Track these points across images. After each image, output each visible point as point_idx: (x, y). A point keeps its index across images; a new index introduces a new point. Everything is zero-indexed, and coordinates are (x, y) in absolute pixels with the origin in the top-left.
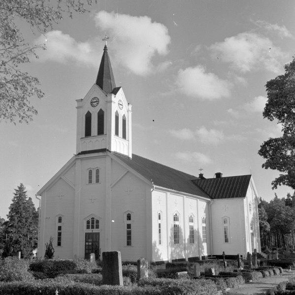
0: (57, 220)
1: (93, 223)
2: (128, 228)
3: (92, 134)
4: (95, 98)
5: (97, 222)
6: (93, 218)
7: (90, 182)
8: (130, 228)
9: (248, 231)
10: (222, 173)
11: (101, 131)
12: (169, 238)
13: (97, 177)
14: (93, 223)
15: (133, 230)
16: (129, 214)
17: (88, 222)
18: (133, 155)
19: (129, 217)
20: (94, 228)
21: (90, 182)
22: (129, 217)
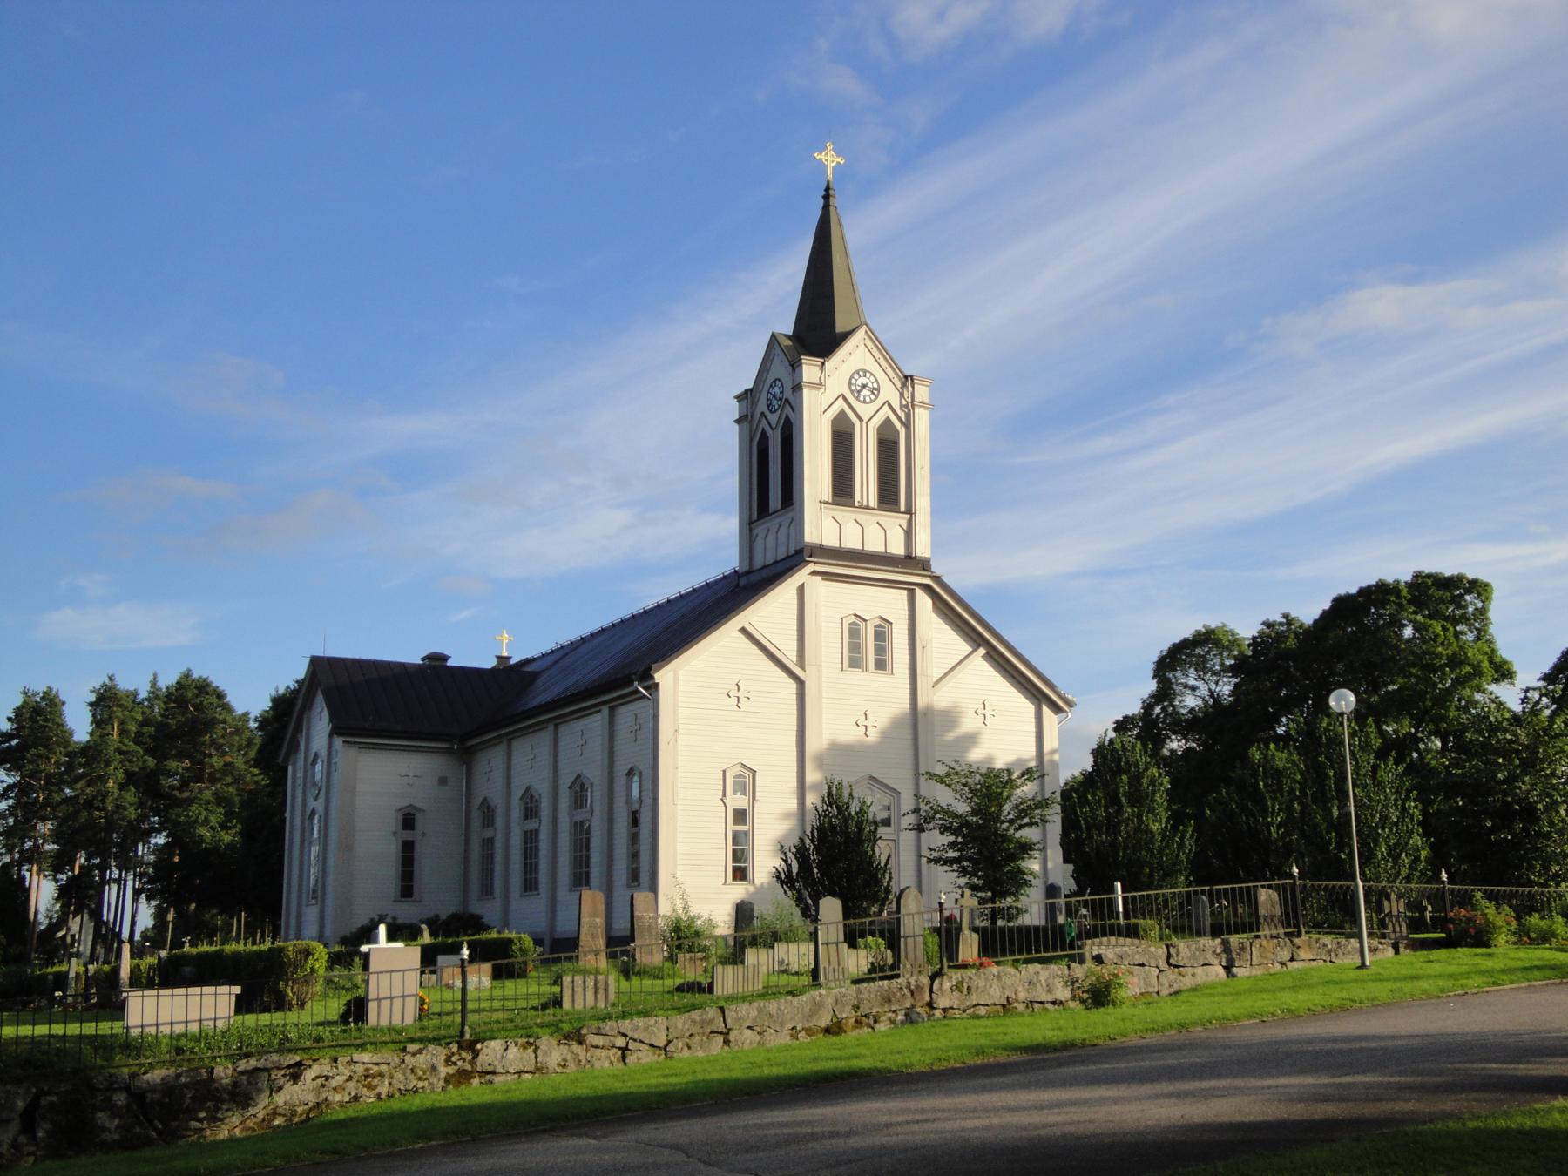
4: (865, 372)
21: (854, 663)
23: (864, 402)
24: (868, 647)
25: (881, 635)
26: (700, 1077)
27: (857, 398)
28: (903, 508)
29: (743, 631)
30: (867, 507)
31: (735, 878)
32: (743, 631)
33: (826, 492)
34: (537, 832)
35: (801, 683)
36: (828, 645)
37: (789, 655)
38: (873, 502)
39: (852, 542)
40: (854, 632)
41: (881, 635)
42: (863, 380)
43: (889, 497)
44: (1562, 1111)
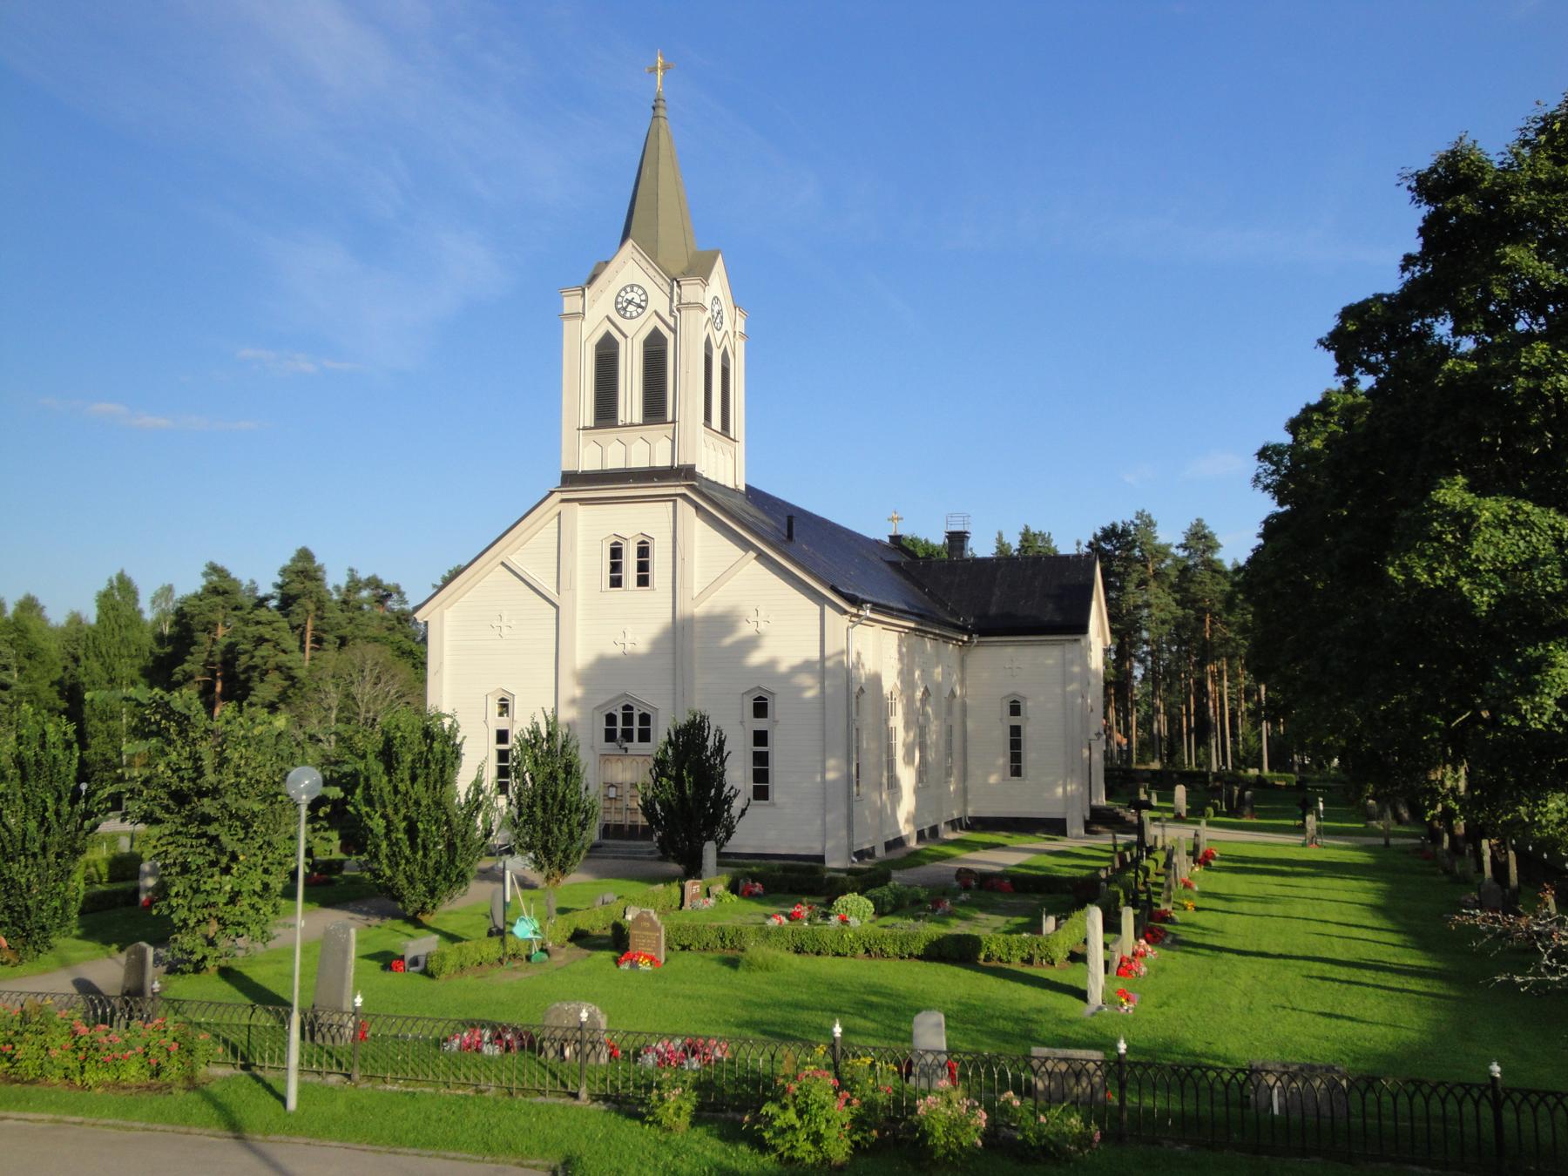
0: (1007, 710)
1: (628, 719)
2: (756, 744)
3: (622, 416)
4: (632, 286)
5: (645, 719)
6: (627, 707)
7: (616, 582)
8: (755, 753)
9: (697, 554)
10: (1122, 515)
11: (655, 408)
12: (458, 1155)
13: (643, 567)
14: (628, 719)
15: (777, 750)
16: (760, 698)
17: (611, 719)
18: (747, 487)
19: (1015, 709)
20: (630, 740)
21: (616, 582)
22: (1015, 709)
23: (631, 318)
24: (629, 565)
25: (643, 551)
26: (629, 648)
27: (624, 316)
28: (670, 418)
29: (503, 564)
30: (632, 425)
31: (766, 798)
32: (503, 564)
33: (588, 416)
34: (1064, 833)
35: (557, 607)
36: (591, 564)
37: (549, 587)
38: (638, 417)
39: (614, 462)
40: (616, 552)
41: (643, 551)
42: (629, 296)
43: (655, 408)
44: (1565, 938)
